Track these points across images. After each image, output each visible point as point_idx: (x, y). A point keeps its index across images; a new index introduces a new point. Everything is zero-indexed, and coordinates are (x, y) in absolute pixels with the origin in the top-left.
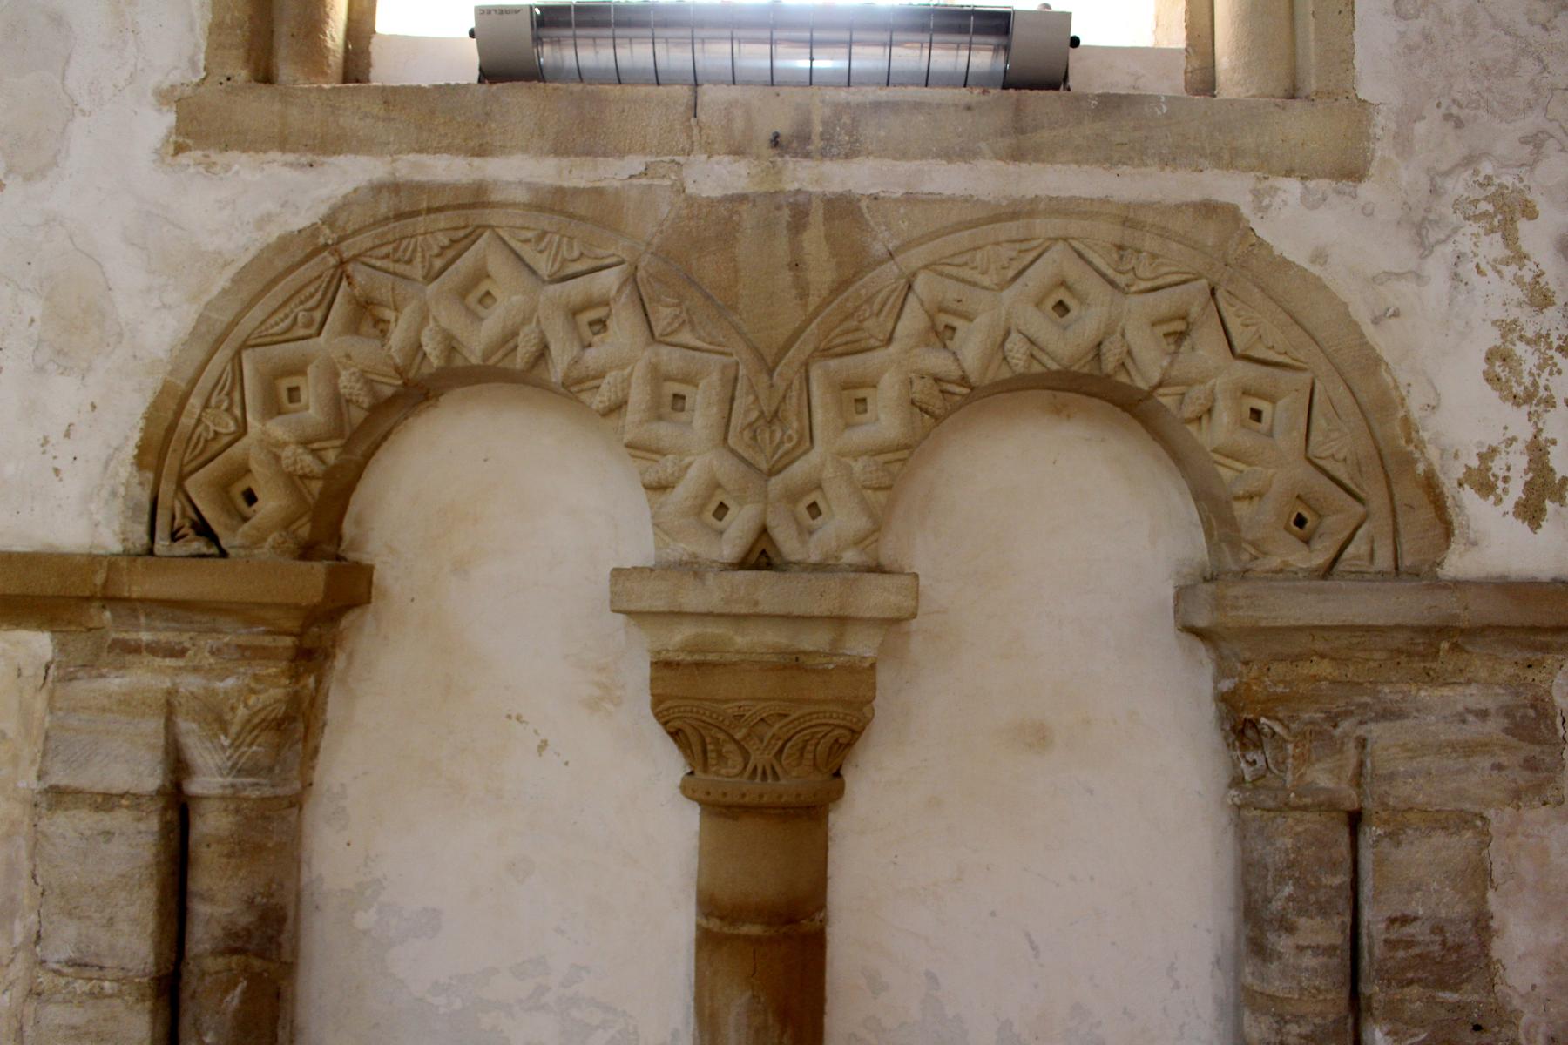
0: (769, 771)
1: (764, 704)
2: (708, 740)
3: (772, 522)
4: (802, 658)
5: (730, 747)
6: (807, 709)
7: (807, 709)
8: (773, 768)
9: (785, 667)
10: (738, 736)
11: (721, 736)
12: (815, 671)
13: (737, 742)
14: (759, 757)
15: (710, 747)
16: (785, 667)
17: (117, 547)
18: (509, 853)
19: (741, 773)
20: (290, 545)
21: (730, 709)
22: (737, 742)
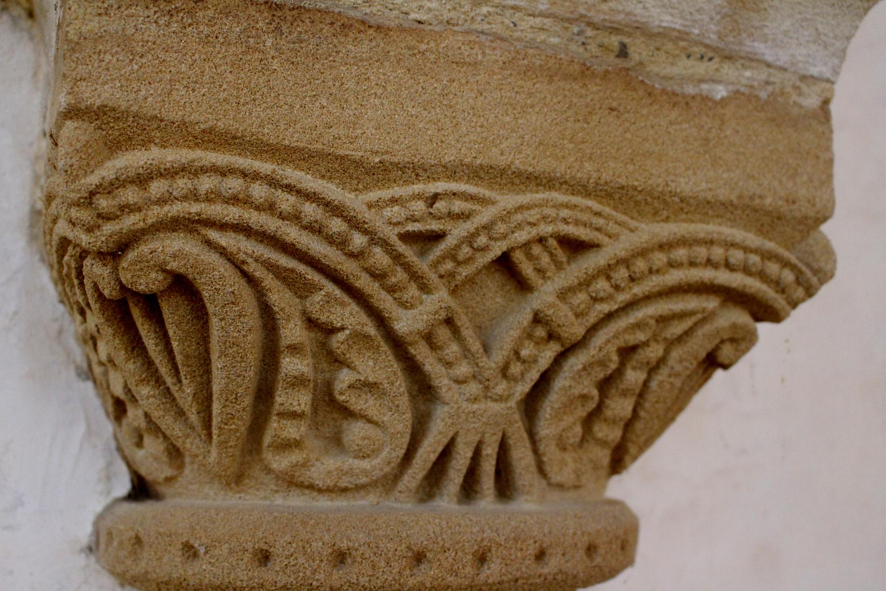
0: (488, 467)
1: (508, 200)
2: (293, 331)
3: (510, 431)
4: (639, 50)
5: (377, 366)
6: (650, 230)
7: (650, 230)
8: (503, 448)
9: (585, 73)
10: (405, 323)
11: (348, 316)
12: (674, 99)
13: (398, 345)
14: (471, 411)
15: (292, 365)
16: (585, 73)
17: (311, 396)
18: (247, 589)
19: (390, 481)
20: (545, 545)
21: (387, 209)
22: (398, 345)
